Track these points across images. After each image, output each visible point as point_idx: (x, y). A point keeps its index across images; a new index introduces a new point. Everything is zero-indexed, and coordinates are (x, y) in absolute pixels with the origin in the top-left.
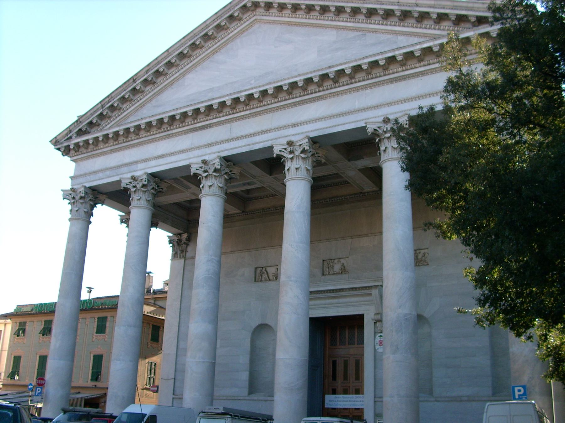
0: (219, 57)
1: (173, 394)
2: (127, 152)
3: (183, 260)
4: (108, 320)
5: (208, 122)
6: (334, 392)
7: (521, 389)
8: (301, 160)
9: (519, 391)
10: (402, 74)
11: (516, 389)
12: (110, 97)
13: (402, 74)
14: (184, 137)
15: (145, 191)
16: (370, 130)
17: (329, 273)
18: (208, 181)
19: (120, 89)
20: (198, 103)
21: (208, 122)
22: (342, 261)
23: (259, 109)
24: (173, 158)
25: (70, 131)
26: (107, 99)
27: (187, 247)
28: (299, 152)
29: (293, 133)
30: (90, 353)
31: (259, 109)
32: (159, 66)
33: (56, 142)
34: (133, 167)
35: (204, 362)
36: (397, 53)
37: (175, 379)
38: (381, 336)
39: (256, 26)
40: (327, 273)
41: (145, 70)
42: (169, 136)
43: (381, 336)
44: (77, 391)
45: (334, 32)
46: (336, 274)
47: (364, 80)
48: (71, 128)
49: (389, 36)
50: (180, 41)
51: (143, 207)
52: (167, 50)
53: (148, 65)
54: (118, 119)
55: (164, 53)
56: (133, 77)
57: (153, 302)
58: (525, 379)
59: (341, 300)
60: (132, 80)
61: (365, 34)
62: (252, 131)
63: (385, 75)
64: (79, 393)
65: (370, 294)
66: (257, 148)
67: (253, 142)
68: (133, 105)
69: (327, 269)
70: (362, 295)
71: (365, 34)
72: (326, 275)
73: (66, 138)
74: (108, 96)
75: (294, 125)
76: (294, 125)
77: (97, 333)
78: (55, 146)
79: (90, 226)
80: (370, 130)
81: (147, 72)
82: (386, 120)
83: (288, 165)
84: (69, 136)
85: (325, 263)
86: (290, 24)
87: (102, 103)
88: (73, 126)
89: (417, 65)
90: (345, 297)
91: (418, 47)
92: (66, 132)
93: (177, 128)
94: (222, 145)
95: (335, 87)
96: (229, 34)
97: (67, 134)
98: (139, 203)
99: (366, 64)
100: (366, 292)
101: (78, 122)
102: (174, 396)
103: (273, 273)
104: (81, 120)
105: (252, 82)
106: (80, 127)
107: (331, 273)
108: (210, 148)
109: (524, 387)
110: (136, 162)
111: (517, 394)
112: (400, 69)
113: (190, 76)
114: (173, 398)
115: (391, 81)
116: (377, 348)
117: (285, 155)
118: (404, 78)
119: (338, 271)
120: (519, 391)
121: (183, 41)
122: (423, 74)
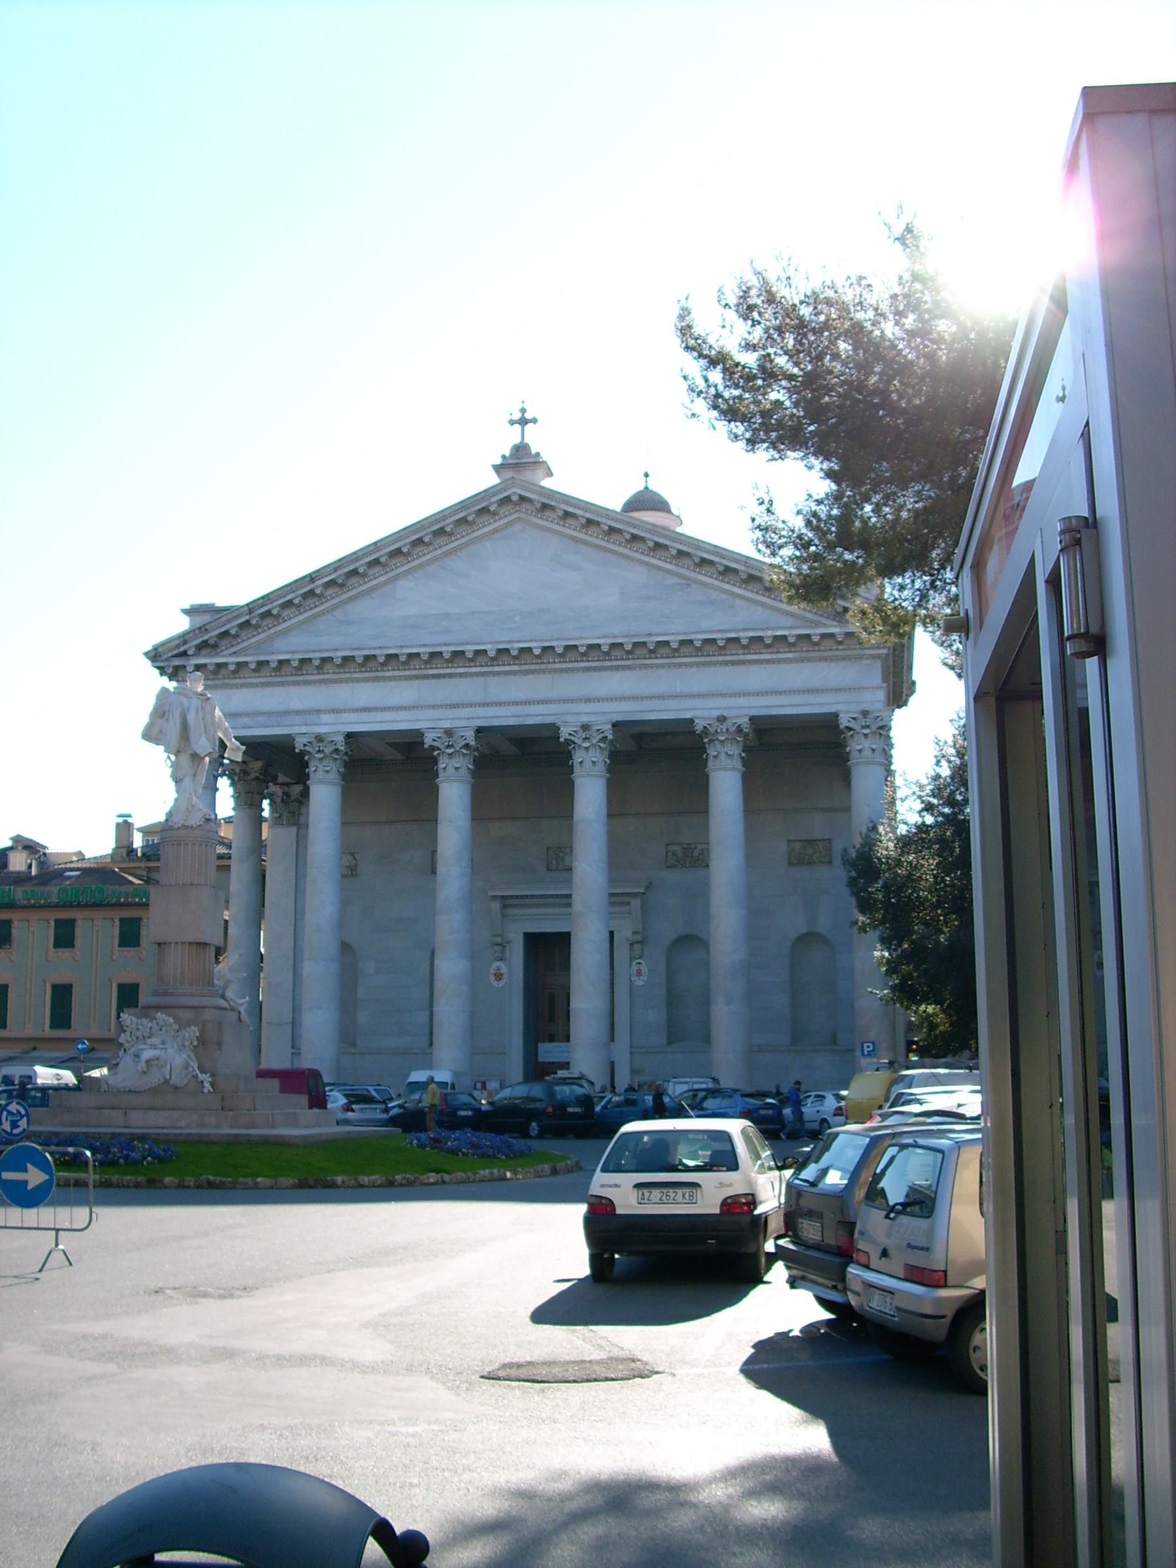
0: (455, 563)
1: (293, 1047)
2: (294, 690)
3: (294, 829)
4: (142, 923)
5: (448, 671)
6: (552, 1039)
7: (870, 1045)
8: (598, 751)
9: (868, 1047)
10: (742, 657)
11: (865, 1045)
12: (266, 599)
13: (742, 657)
14: (405, 683)
15: (336, 759)
16: (699, 728)
17: (557, 867)
18: (453, 761)
19: (286, 589)
20: (440, 645)
21: (448, 671)
23: (533, 667)
24: (388, 716)
25: (185, 642)
26: (260, 602)
27: (299, 808)
28: (597, 739)
29: (587, 711)
30: (110, 981)
31: (533, 667)
32: (358, 564)
33: (146, 654)
34: (313, 718)
35: (463, 1011)
36: (742, 635)
37: (293, 1023)
38: (639, 963)
39: (518, 527)
40: (555, 867)
41: (333, 567)
42: (376, 679)
43: (639, 963)
44: (32, 1046)
45: (644, 570)
47: (691, 656)
48: (187, 637)
49: (723, 596)
50: (398, 532)
51: (335, 784)
52: (375, 543)
53: (340, 560)
54: (272, 631)
55: (368, 546)
56: (310, 575)
57: (145, 874)
58: (872, 1035)
59: (534, 911)
60: (309, 579)
61: (689, 585)
62: (521, 696)
63: (720, 655)
64: (35, 1049)
65: (629, 903)
66: (532, 722)
67: (526, 713)
68: (301, 614)
69: (554, 862)
71: (689, 585)
72: (552, 870)
73: (175, 652)
74: (263, 598)
75: (588, 700)
76: (588, 700)
77: (121, 945)
78: (153, 661)
79: (217, 793)
80: (699, 728)
81: (336, 570)
82: (722, 719)
83: (578, 756)
84: (182, 649)
85: (551, 853)
86: (574, 539)
87: (251, 606)
88: (192, 634)
89: (764, 651)
91: (770, 633)
92: (177, 642)
93: (394, 670)
94: (473, 709)
95: (651, 658)
96: (474, 531)
97: (178, 646)
98: (327, 776)
99: (699, 640)
100: (625, 899)
101: (203, 630)
102: (293, 1051)
104: (207, 627)
105: (517, 618)
106: (205, 638)
107: (561, 867)
108: (453, 710)
109: (873, 1043)
110: (319, 711)
111: (866, 1050)
112: (740, 652)
113: (404, 584)
114: (293, 1054)
115: (726, 663)
116: (633, 979)
117: (576, 740)
118: (744, 662)
120: (868, 1047)
121: (402, 533)
122: (768, 661)
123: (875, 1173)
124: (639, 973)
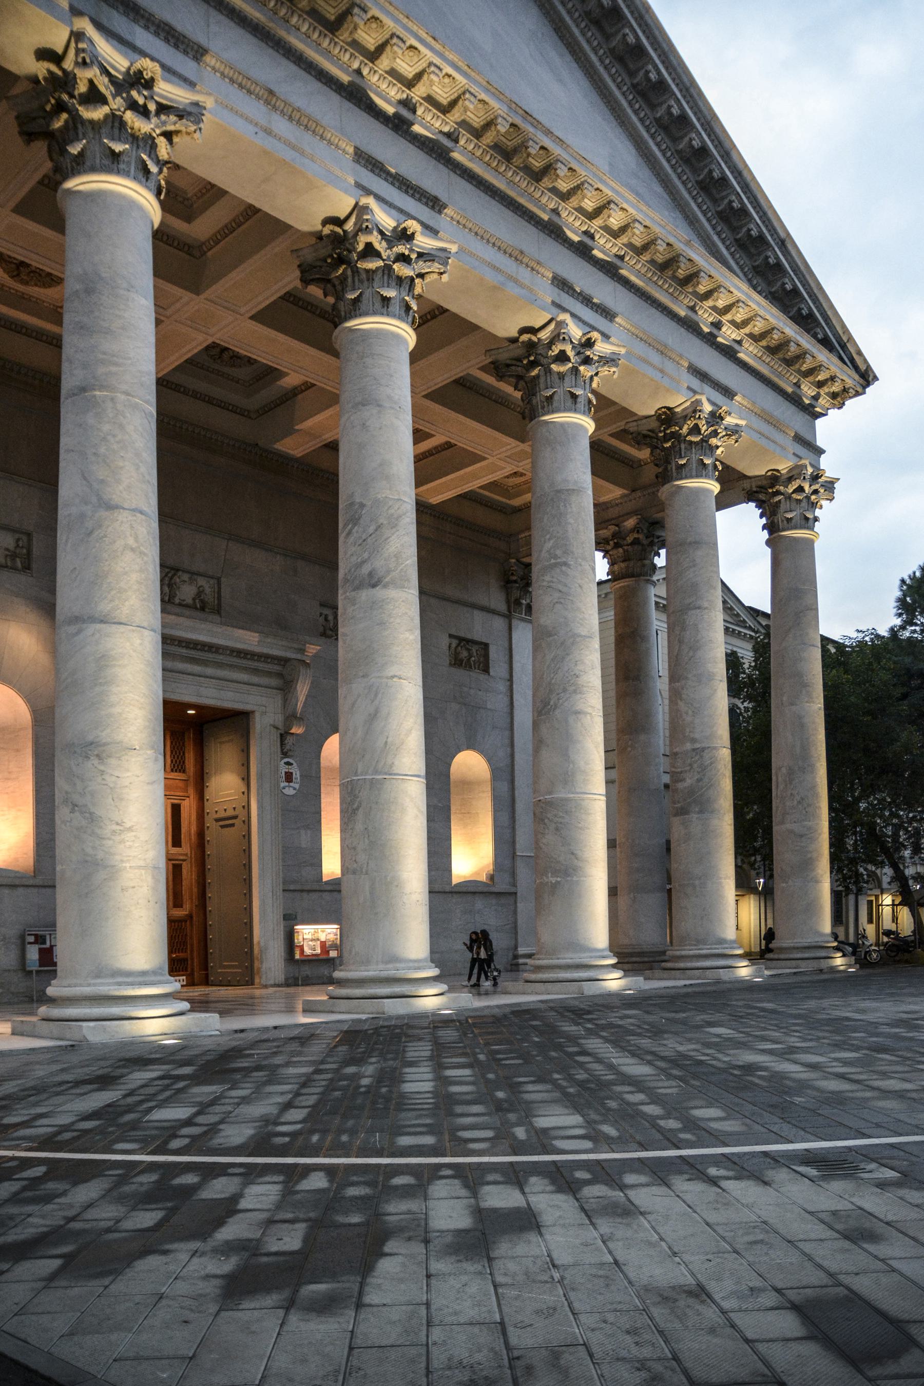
22: (202, 581)
46: (187, 606)
59: (209, 671)
70: (256, 671)
90: (220, 665)
103: (7, 549)
119: (189, 601)
123: (192, 1010)
124: (289, 777)
